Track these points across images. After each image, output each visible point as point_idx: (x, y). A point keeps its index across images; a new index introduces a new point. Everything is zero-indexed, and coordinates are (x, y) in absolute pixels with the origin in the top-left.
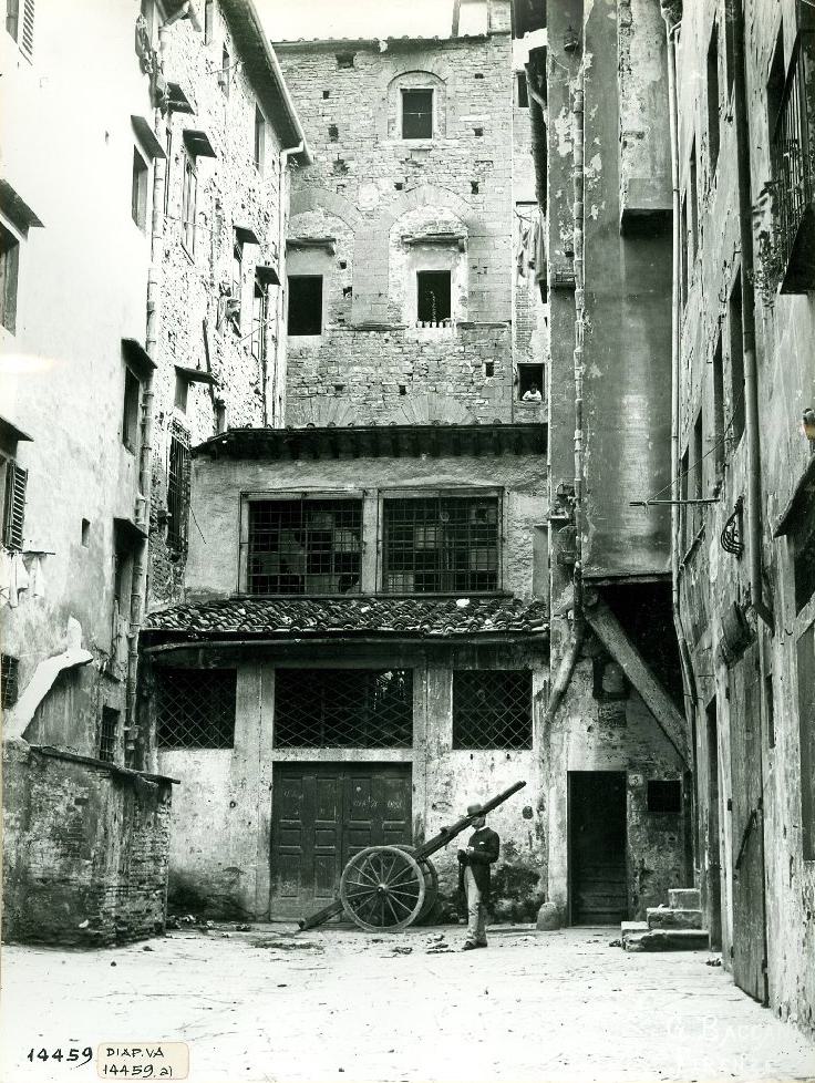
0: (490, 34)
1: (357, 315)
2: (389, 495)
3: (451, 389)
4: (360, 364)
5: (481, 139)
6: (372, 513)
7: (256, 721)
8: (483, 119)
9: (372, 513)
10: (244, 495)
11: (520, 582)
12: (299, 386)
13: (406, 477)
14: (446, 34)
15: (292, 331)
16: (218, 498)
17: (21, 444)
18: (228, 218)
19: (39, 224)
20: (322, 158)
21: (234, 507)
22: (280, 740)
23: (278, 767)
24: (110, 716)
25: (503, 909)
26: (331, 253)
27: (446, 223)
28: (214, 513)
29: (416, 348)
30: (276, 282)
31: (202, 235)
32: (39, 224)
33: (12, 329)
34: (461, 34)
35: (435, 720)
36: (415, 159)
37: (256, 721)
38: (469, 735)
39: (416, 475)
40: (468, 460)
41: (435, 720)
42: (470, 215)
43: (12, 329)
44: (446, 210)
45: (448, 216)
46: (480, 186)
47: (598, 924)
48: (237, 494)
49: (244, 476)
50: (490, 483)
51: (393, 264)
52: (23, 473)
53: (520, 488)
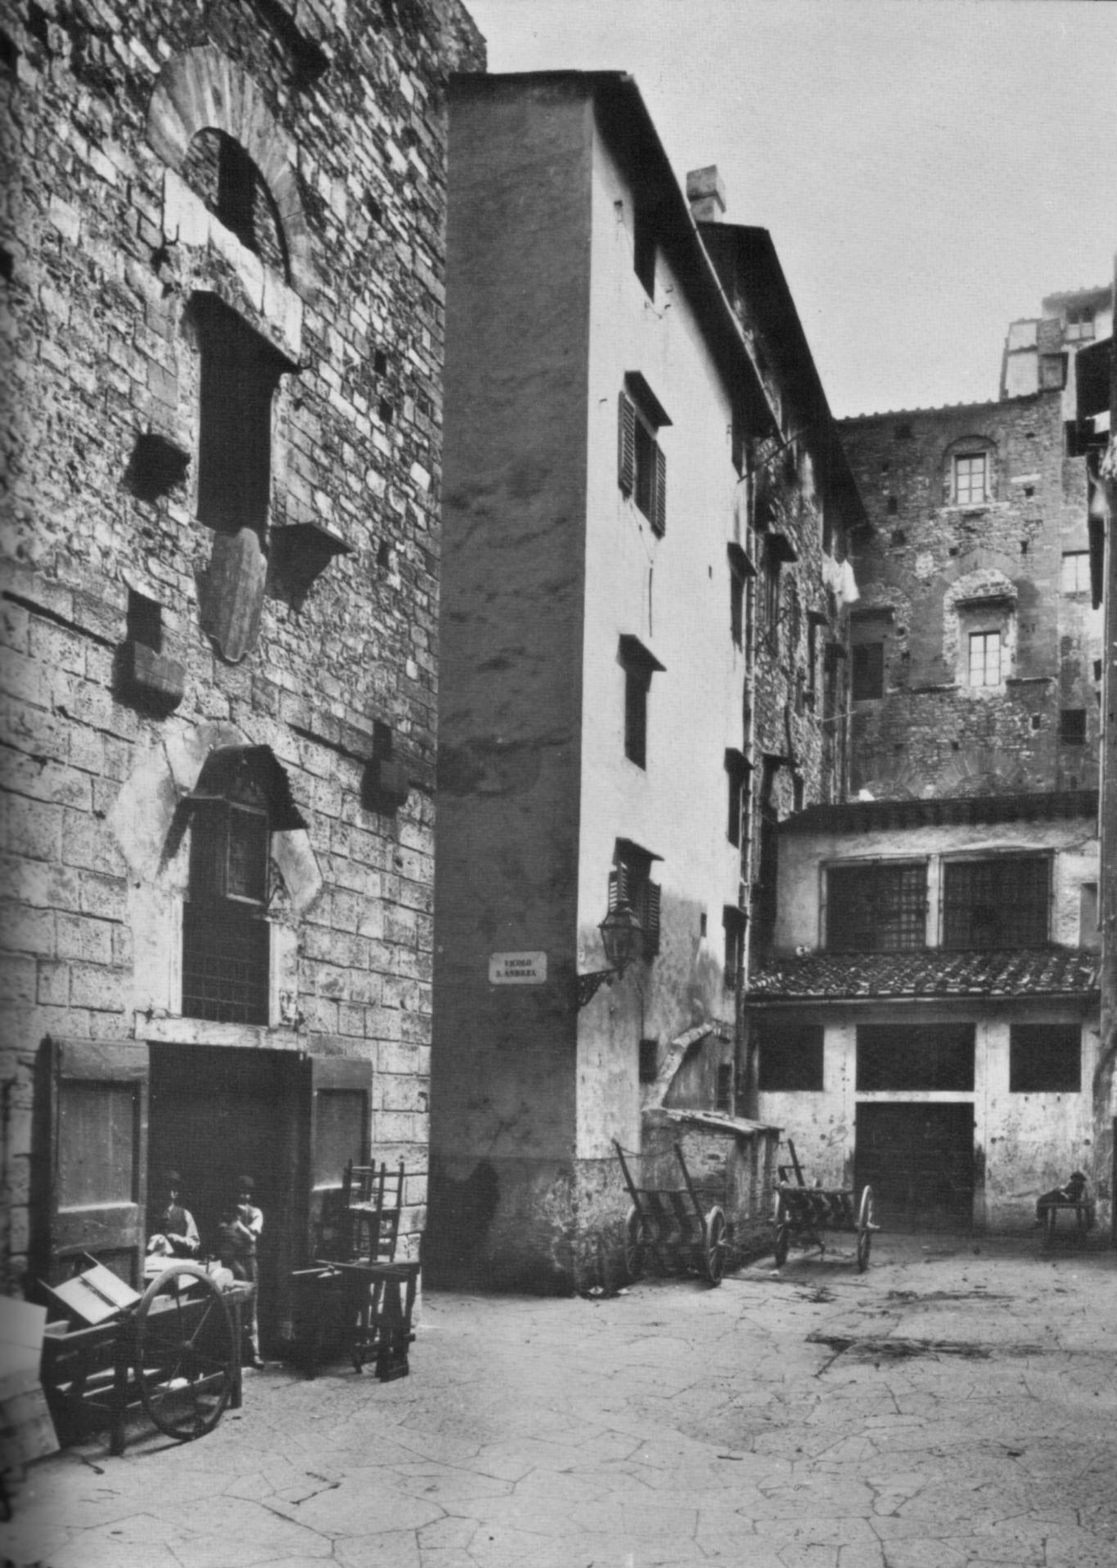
0: (1041, 392)
1: (916, 678)
2: (950, 860)
3: (1000, 743)
5: (1032, 499)
8: (1033, 478)
11: (1069, 934)
13: (965, 843)
14: (995, 398)
17: (655, 864)
19: (661, 668)
24: (724, 1070)
26: (890, 621)
27: (998, 584)
29: (966, 706)
32: (661, 668)
34: (1012, 395)
36: (969, 524)
38: (1023, 1080)
39: (973, 841)
40: (1021, 825)
42: (1020, 574)
44: (997, 572)
45: (999, 577)
46: (1030, 545)
47: (945, 919)
48: (816, 863)
51: (947, 627)
53: (1070, 849)
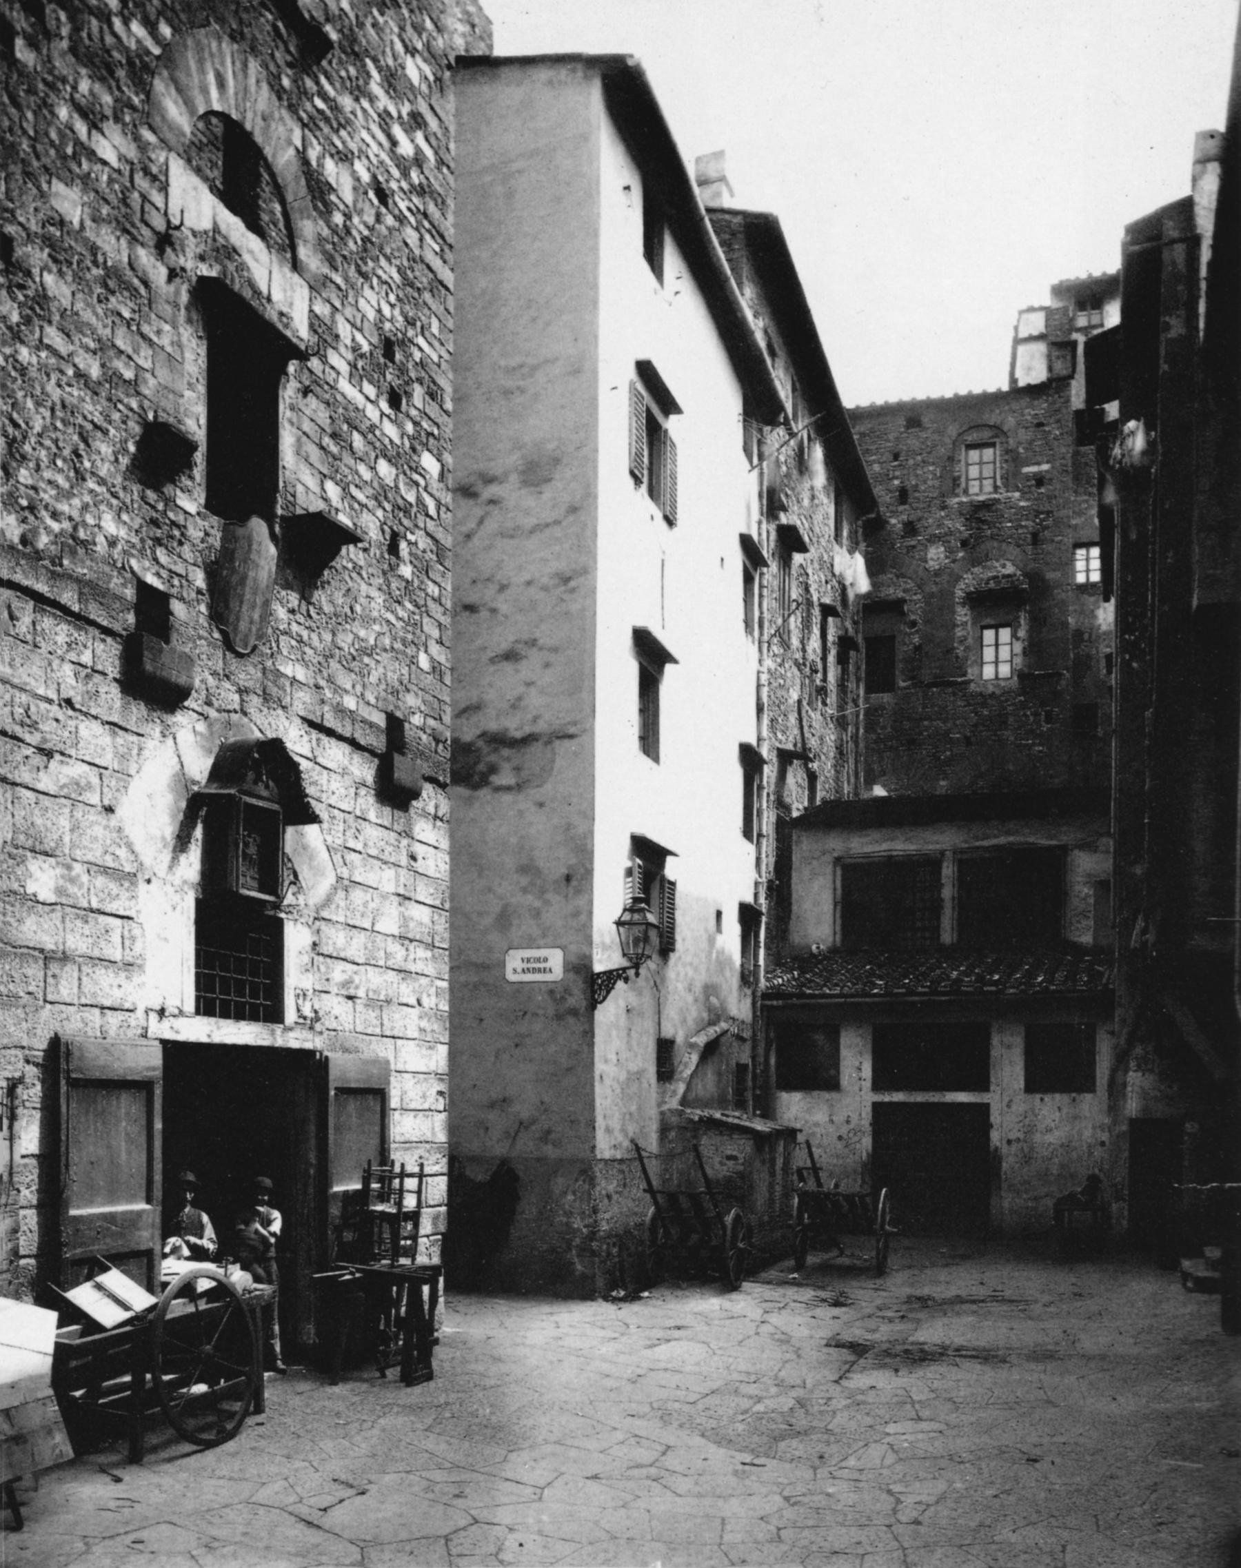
4: (929, 719)
6: (948, 871)
7: (855, 1062)
9: (948, 871)
10: (838, 860)
12: (876, 742)
15: (987, 1106)
16: (815, 862)
17: (669, 859)
18: (815, 599)
19: (675, 661)
20: (893, 521)
21: (829, 869)
22: (877, 1086)
23: (876, 1106)
25: (932, 565)
28: (814, 874)
30: (857, 650)
31: (794, 622)
32: (675, 661)
33: (656, 759)
35: (1009, 1065)
37: (855, 1062)
41: (1009, 1065)
43: (656, 759)
49: (836, 844)
50: (1054, 842)
52: (673, 884)
